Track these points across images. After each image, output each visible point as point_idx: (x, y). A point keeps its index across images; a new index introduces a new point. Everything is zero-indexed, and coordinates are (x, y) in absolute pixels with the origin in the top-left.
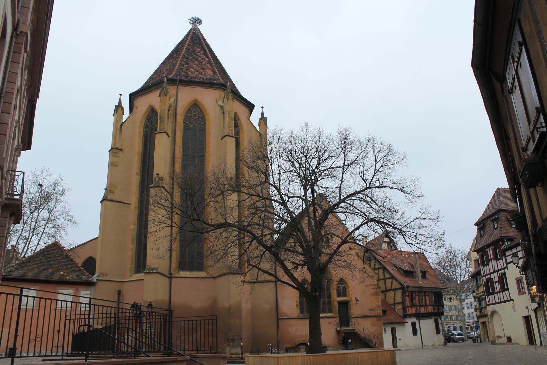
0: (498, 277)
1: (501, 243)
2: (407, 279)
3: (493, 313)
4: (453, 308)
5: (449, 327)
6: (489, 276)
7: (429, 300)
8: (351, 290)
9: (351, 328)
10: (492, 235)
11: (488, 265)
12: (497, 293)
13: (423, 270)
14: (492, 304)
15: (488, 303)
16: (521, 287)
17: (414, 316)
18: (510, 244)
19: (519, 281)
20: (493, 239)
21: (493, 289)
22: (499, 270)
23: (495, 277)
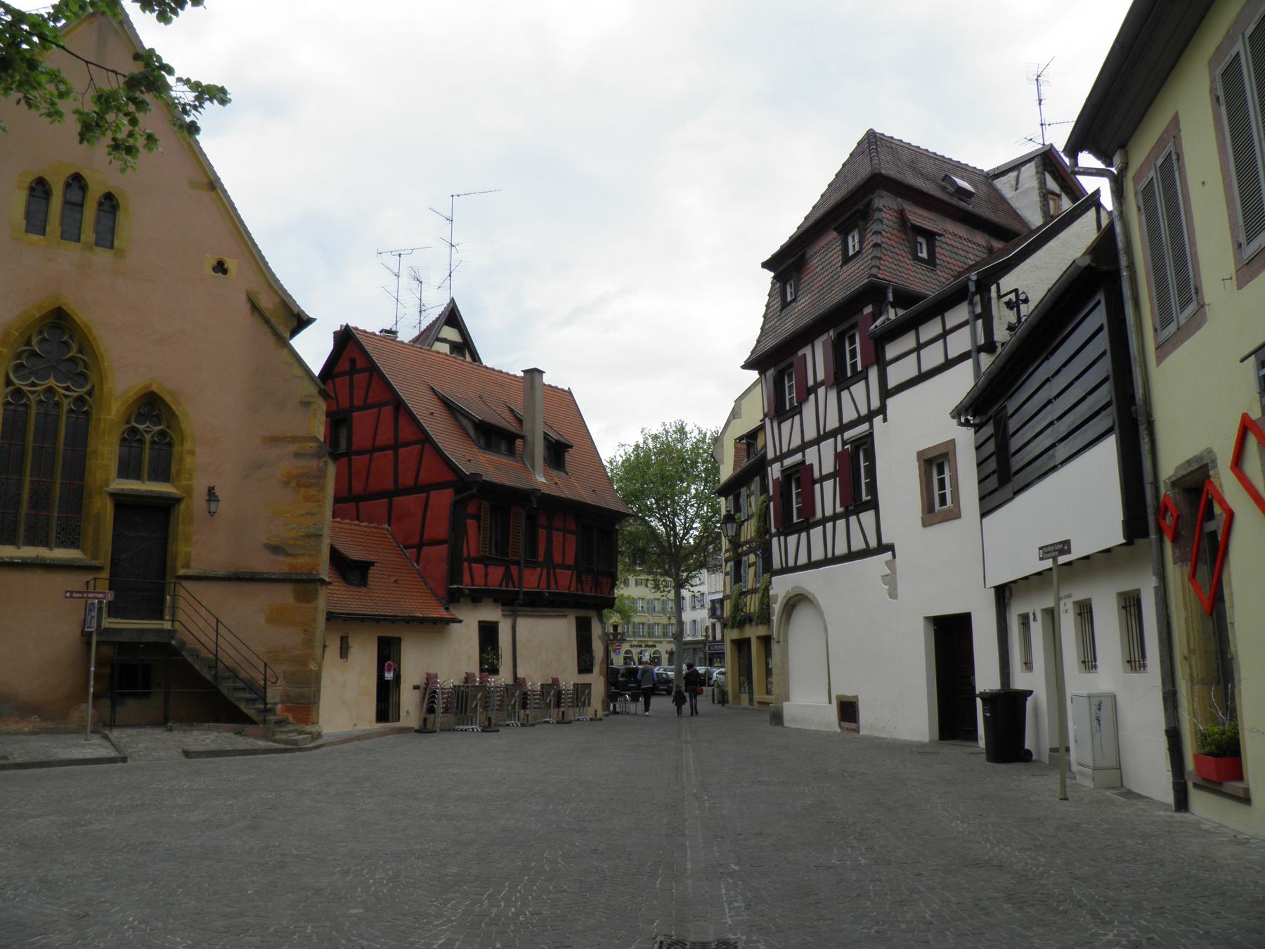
0: (837, 455)
1: (868, 310)
3: (797, 601)
4: (658, 606)
5: (641, 653)
6: (797, 458)
7: (564, 546)
8: (192, 452)
11: (800, 413)
12: (824, 521)
13: (555, 436)
14: (796, 568)
15: (776, 564)
16: (936, 493)
17: (496, 601)
20: (836, 296)
22: (843, 428)
23: (824, 458)
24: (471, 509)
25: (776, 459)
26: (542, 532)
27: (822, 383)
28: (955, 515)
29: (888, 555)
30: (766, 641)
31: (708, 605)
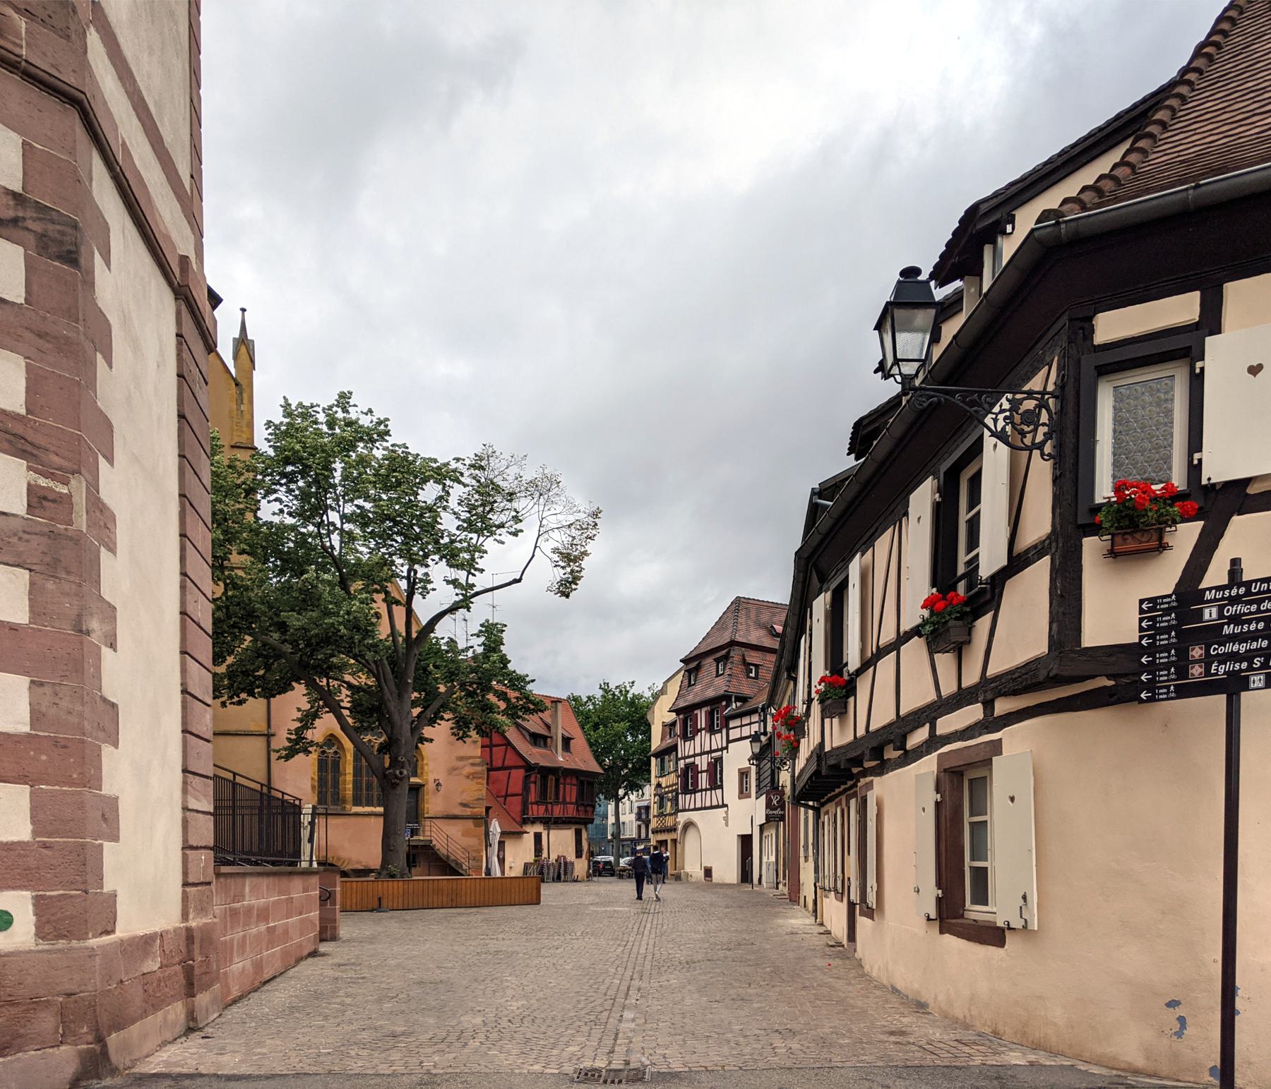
0: (708, 763)
1: (724, 703)
2: (536, 750)
3: (689, 825)
6: (691, 760)
8: (427, 764)
9: (421, 838)
10: (711, 684)
12: (701, 790)
15: (680, 808)
17: (541, 822)
18: (741, 706)
19: (744, 774)
20: (710, 693)
21: (695, 783)
22: (711, 751)
23: (703, 763)
24: (532, 779)
25: (682, 758)
26: (561, 786)
27: (704, 729)
28: (749, 796)
29: (726, 809)
30: (674, 841)
31: (635, 810)
